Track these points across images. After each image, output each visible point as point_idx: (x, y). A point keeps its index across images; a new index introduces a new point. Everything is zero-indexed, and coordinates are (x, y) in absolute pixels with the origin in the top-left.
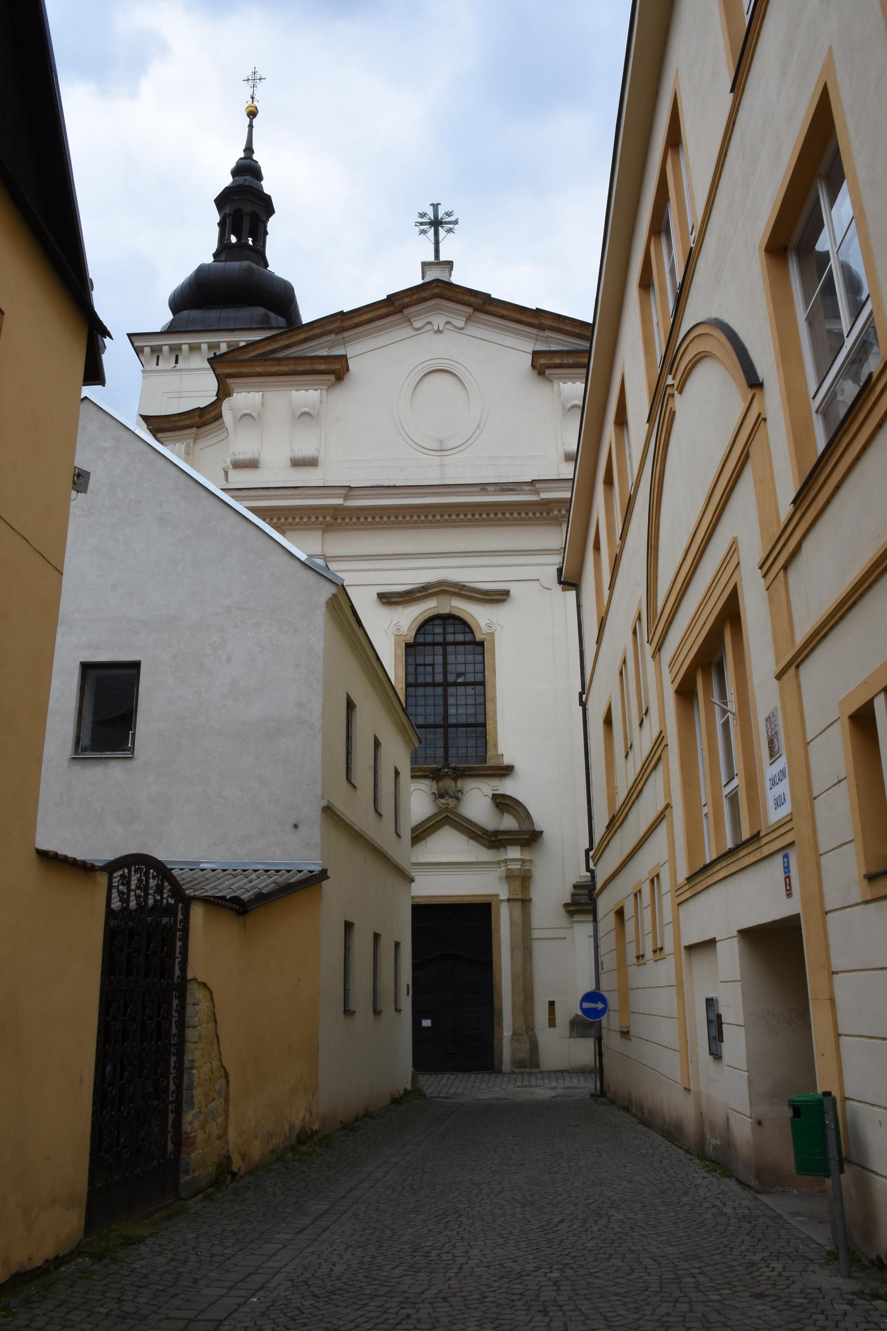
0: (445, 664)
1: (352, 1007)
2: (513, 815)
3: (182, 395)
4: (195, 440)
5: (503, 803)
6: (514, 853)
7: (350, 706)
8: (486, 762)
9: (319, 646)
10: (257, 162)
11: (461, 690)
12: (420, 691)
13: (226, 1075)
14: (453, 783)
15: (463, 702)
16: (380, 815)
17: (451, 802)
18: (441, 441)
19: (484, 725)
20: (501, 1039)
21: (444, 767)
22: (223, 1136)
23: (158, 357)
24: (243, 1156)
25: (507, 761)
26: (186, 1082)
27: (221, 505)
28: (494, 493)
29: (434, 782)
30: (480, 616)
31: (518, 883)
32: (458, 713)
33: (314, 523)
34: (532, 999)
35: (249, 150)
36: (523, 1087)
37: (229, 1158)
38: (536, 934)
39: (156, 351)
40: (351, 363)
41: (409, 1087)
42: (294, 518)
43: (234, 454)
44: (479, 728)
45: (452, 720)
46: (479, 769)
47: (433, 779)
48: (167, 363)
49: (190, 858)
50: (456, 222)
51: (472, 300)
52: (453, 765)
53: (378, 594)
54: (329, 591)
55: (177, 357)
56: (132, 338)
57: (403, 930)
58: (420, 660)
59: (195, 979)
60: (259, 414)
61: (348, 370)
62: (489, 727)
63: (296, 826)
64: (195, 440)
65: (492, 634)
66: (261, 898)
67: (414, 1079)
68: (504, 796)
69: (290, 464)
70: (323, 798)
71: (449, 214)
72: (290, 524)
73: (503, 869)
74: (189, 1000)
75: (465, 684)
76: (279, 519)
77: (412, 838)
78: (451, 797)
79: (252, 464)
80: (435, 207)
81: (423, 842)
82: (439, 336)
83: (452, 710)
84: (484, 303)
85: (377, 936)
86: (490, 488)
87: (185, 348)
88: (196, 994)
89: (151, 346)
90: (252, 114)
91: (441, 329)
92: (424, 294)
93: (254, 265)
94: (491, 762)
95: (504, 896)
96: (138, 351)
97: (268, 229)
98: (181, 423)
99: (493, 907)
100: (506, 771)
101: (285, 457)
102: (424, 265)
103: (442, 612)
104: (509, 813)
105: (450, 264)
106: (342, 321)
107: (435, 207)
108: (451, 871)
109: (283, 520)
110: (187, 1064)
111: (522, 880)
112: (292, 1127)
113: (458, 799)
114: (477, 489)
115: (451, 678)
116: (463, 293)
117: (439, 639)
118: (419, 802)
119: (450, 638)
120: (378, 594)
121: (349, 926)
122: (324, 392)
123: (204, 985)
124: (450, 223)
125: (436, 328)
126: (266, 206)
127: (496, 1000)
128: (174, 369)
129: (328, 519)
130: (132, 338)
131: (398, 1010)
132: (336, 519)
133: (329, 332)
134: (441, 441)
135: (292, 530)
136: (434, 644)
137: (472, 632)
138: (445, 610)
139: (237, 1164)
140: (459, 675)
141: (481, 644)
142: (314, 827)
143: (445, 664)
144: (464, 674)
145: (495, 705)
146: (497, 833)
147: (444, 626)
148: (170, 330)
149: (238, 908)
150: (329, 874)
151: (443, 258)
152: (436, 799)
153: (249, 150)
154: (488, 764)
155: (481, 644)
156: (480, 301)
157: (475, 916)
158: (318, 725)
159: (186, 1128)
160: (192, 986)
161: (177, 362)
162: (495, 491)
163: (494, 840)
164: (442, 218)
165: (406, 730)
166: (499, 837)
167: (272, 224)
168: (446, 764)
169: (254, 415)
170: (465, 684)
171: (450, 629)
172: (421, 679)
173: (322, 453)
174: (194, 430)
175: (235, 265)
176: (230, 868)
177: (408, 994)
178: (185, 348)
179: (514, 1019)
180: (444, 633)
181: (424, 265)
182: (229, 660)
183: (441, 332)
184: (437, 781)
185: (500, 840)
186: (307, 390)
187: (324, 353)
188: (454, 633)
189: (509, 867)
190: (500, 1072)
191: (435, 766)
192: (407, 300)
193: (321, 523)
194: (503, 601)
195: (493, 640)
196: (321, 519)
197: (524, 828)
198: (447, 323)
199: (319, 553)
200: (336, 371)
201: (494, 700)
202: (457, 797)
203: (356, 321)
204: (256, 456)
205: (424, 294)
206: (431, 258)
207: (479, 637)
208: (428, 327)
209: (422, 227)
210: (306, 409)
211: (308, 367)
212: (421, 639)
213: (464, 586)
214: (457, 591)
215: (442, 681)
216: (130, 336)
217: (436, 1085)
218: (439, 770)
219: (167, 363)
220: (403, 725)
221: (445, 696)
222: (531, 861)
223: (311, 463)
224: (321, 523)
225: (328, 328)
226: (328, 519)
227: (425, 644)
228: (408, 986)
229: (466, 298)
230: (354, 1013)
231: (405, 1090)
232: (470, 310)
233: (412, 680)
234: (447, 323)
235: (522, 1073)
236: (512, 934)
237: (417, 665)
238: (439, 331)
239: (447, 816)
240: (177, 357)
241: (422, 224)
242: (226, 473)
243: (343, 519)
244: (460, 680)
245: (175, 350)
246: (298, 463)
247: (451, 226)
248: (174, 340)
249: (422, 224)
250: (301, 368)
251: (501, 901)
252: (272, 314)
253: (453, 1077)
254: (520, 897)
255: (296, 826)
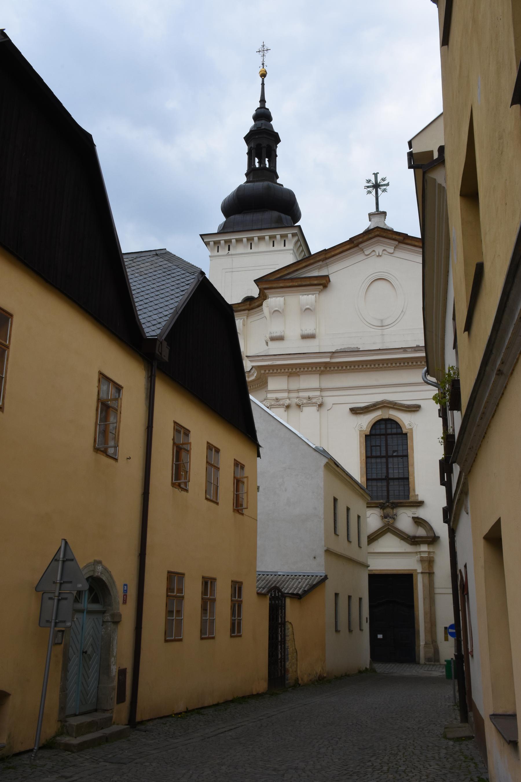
0: (387, 446)
1: (339, 629)
2: (423, 528)
3: (234, 270)
4: (247, 317)
5: (418, 521)
6: (424, 548)
7: (335, 500)
8: (409, 499)
9: (322, 484)
10: (268, 109)
11: (395, 459)
12: (373, 460)
13: (297, 652)
14: (391, 510)
15: (397, 466)
16: (350, 542)
17: (391, 521)
18: (382, 321)
19: (408, 479)
20: (419, 646)
21: (387, 503)
22: (296, 671)
23: (218, 247)
24: (302, 679)
25: (420, 499)
26: (286, 653)
27: (279, 423)
28: (411, 352)
29: (382, 510)
30: (405, 420)
31: (426, 564)
32: (394, 473)
33: (314, 371)
34: (435, 626)
35: (263, 101)
36: (428, 670)
37: (298, 679)
38: (437, 591)
39: (217, 243)
40: (331, 278)
41: (368, 667)
42: (304, 369)
43: (271, 333)
44: (405, 480)
45: (391, 476)
46: (406, 503)
47: (381, 508)
48: (223, 251)
49: (274, 570)
50: (388, 185)
51: (397, 237)
52: (391, 501)
53: (350, 409)
54: (324, 461)
55: (229, 246)
56: (203, 237)
57: (364, 591)
58: (373, 444)
59: (288, 621)
60: (283, 310)
61: (330, 281)
62: (411, 480)
63: (315, 558)
64: (247, 317)
65: (411, 429)
66: (306, 592)
67: (371, 664)
68: (418, 518)
69: (300, 338)
70: (325, 546)
71: (383, 180)
72: (302, 371)
73: (419, 556)
74: (286, 628)
75: (397, 456)
76: (296, 369)
77: (368, 541)
78: (391, 518)
79: (281, 338)
80: (376, 175)
81: (377, 541)
82: (379, 258)
83: (390, 471)
84: (404, 239)
85: (350, 597)
86: (408, 350)
87: (234, 241)
88: (288, 626)
89: (214, 241)
90: (263, 75)
91: (380, 254)
92: (370, 236)
93: (270, 183)
94: (412, 499)
95: (419, 571)
96: (207, 244)
97: (276, 130)
98: (239, 308)
99: (414, 576)
100: (420, 504)
101: (298, 333)
102: (370, 215)
103: (384, 417)
104: (421, 526)
105: (384, 213)
106: (326, 254)
107: (376, 175)
108: (391, 556)
109: (298, 370)
110: (286, 647)
111: (429, 562)
112: (316, 673)
113: (394, 519)
114: (402, 350)
115: (390, 453)
116: (392, 234)
117: (383, 431)
118: (373, 520)
119: (389, 431)
120: (350, 409)
121: (337, 595)
122: (317, 295)
123: (290, 623)
124: (384, 185)
125: (378, 254)
126: (276, 139)
127: (416, 625)
128: (228, 255)
129: (322, 368)
130: (203, 237)
131: (361, 630)
132: (326, 368)
133: (319, 261)
134: (382, 321)
135: (303, 374)
136: (380, 435)
137: (401, 428)
138: (386, 417)
139: (300, 682)
140: (394, 451)
141: (406, 434)
142: (322, 559)
143: (387, 446)
144: (397, 451)
145: (414, 468)
146: (414, 537)
147: (386, 424)
148: (224, 230)
149: (298, 597)
150: (328, 577)
151: (381, 209)
152: (382, 519)
153: (263, 101)
154: (410, 500)
155: (406, 434)
156: (402, 238)
157: (405, 580)
158: (322, 517)
159: (287, 667)
160: (287, 624)
161: (229, 250)
162: (411, 351)
163: (414, 541)
164: (380, 183)
165: (363, 495)
166: (416, 540)
167: (280, 149)
168: (388, 501)
169: (280, 310)
170: (397, 456)
171: (389, 426)
172: (374, 454)
173: (317, 330)
174: (247, 312)
175: (260, 185)
176: (290, 574)
177: (367, 622)
178: (234, 241)
179: (425, 636)
180: (386, 429)
181: (370, 215)
182: (286, 490)
183: (381, 256)
184: (383, 510)
185: (417, 541)
186: (308, 295)
187: (315, 273)
188: (391, 428)
189: (422, 555)
190: (419, 663)
191: (382, 501)
192: (360, 240)
193: (319, 371)
194: (418, 411)
195: (412, 433)
196: (318, 369)
197: (429, 535)
198: (384, 250)
199: (318, 387)
200: (323, 283)
201: (413, 465)
202: (394, 518)
203: (333, 253)
204: (282, 334)
205: (370, 236)
206: (374, 210)
207: (404, 431)
208: (373, 253)
209: (369, 189)
210: (308, 307)
211: (308, 283)
212: (373, 432)
213: (396, 403)
214: (392, 406)
215: (385, 455)
216: (201, 235)
217: (381, 668)
218: (384, 504)
219: (223, 251)
220: (362, 494)
221: (387, 463)
222: (434, 552)
223: (312, 336)
224: (319, 371)
225: (318, 259)
226: (322, 368)
227: (376, 435)
228: (367, 618)
229: (394, 236)
230: (339, 631)
231: (366, 668)
232: (397, 243)
233: (369, 455)
234: (384, 250)
235: (430, 665)
236: (424, 591)
237: (372, 446)
238: (379, 256)
239: (388, 528)
240: (229, 246)
241: (368, 187)
242: (267, 343)
243: (330, 368)
244: (395, 454)
245: (228, 242)
246: (305, 337)
247: (385, 187)
248: (227, 237)
249: (368, 187)
250: (304, 283)
251: (418, 573)
252: (283, 215)
253: (393, 665)
254: (427, 571)
255: (315, 558)
